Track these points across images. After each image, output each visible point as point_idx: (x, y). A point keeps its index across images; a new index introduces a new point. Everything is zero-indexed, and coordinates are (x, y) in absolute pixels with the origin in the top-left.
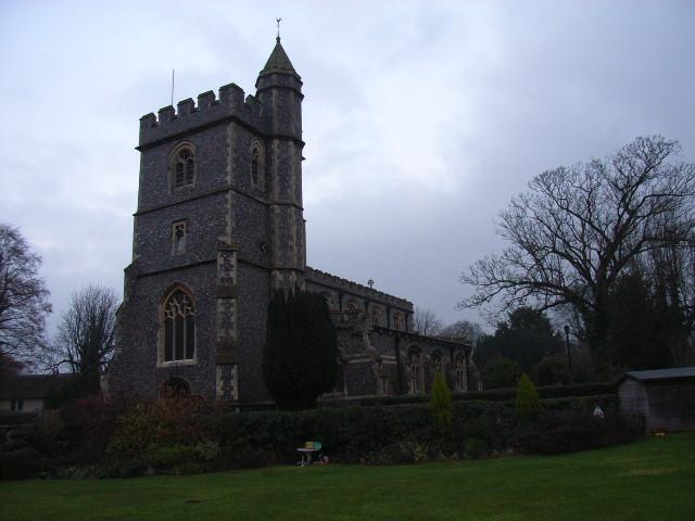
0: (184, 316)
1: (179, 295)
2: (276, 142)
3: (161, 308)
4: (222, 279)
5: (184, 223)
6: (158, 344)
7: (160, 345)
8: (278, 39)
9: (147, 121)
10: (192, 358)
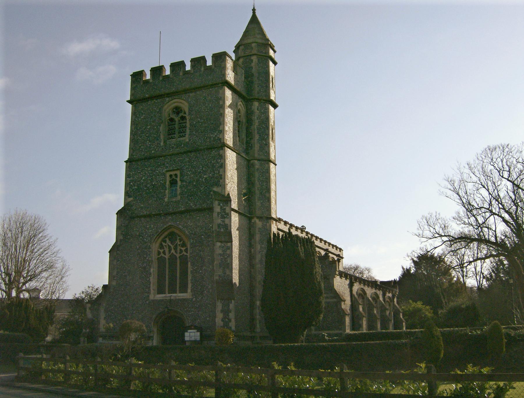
0: (178, 256)
1: (172, 236)
2: (256, 104)
3: (155, 247)
4: (219, 225)
5: (178, 172)
6: (151, 278)
7: (153, 279)
8: (254, 10)
9: (137, 77)
10: (186, 292)
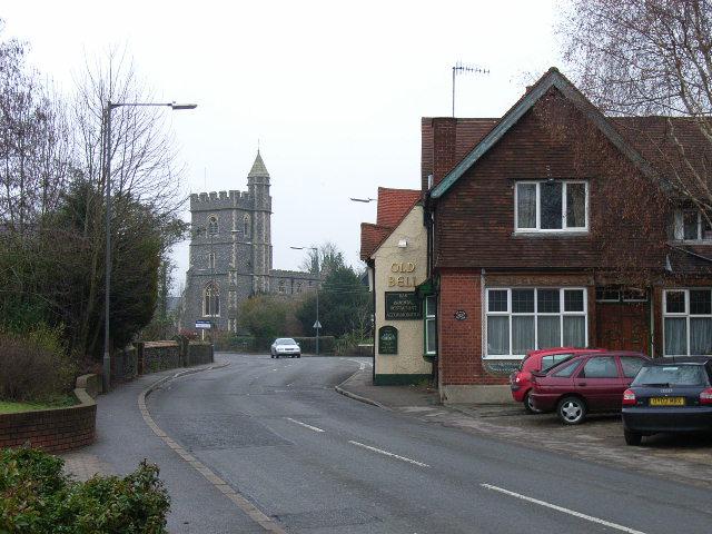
7: (204, 307)
